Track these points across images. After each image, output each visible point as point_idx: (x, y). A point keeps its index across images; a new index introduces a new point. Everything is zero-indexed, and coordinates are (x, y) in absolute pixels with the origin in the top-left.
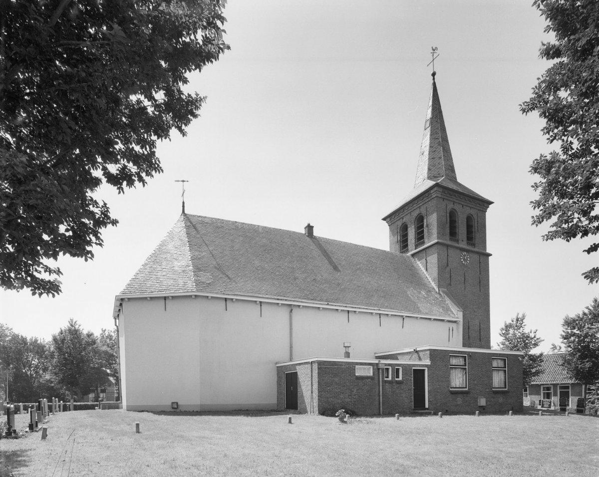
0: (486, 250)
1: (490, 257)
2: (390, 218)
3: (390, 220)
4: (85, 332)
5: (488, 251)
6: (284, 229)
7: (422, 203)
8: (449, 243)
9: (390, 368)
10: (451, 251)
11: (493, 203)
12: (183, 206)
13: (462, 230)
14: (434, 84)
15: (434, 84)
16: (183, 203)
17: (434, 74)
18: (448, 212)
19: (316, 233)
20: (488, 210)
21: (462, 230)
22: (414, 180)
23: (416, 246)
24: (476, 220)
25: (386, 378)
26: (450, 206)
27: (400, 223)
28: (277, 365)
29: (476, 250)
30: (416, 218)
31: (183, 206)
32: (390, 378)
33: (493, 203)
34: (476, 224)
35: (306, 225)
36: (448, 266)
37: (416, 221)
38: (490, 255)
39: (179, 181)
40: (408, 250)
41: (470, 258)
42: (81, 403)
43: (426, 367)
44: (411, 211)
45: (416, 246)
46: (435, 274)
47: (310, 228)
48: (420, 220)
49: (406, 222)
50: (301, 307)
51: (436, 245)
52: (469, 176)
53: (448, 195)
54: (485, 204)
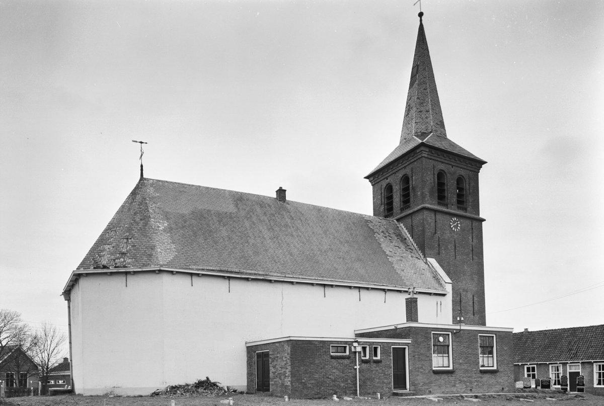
0: (478, 214)
1: (483, 222)
2: (373, 177)
5: (482, 216)
6: (477, 156)
9: (535, 366)
10: (439, 216)
11: (486, 163)
12: (142, 170)
13: (451, 193)
14: (421, 28)
15: (421, 28)
16: (142, 166)
17: (421, 15)
18: (436, 173)
19: (288, 197)
21: (451, 193)
22: (386, 140)
23: (402, 210)
24: (467, 182)
25: (363, 357)
27: (384, 184)
29: (468, 214)
30: (401, 179)
31: (142, 170)
32: (367, 357)
33: (486, 163)
36: (435, 233)
37: (401, 182)
38: (484, 220)
39: (136, 142)
40: (392, 214)
41: (461, 224)
42: (60, 389)
43: (406, 345)
47: (281, 192)
49: (396, 185)
50: (200, 275)
52: (461, 133)
53: (436, 155)
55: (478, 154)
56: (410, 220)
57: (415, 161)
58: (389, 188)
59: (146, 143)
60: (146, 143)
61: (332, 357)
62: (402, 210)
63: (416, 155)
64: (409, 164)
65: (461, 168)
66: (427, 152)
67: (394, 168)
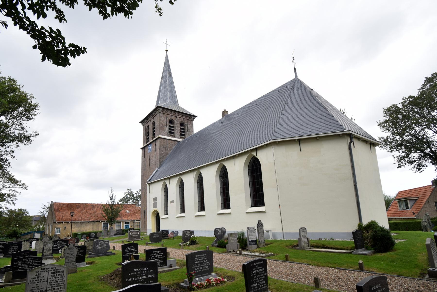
2: (142, 122)
11: (196, 117)
12: (295, 71)
14: (167, 57)
15: (167, 57)
16: (295, 69)
17: (167, 51)
23: (153, 138)
27: (147, 125)
31: (295, 71)
33: (196, 117)
55: (192, 112)
58: (148, 127)
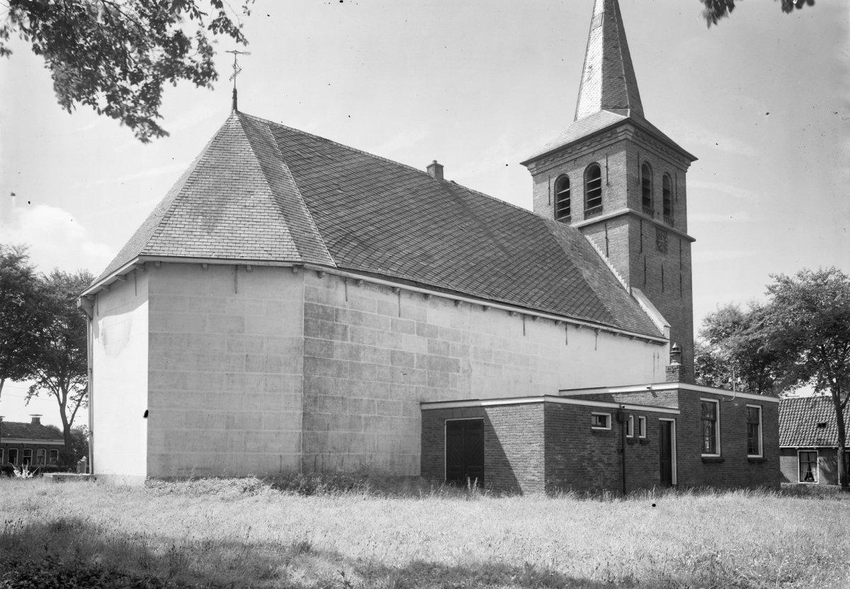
0: (686, 232)
3: (536, 165)
4: (766, 301)
5: (690, 233)
7: (599, 147)
8: (640, 213)
12: (235, 98)
16: (235, 92)
20: (690, 169)
22: (590, 110)
23: (587, 215)
26: (645, 157)
28: (425, 407)
31: (235, 98)
33: (697, 159)
34: (674, 189)
35: (431, 163)
38: (693, 240)
44: (576, 156)
45: (587, 215)
46: (625, 263)
48: (594, 172)
51: (628, 217)
54: (686, 160)
56: (604, 233)
57: (612, 145)
58: (564, 183)
59: (228, 52)
60: (228, 52)
61: (594, 432)
62: (587, 215)
63: (614, 136)
64: (601, 149)
65: (668, 162)
66: (630, 132)
67: (574, 153)
